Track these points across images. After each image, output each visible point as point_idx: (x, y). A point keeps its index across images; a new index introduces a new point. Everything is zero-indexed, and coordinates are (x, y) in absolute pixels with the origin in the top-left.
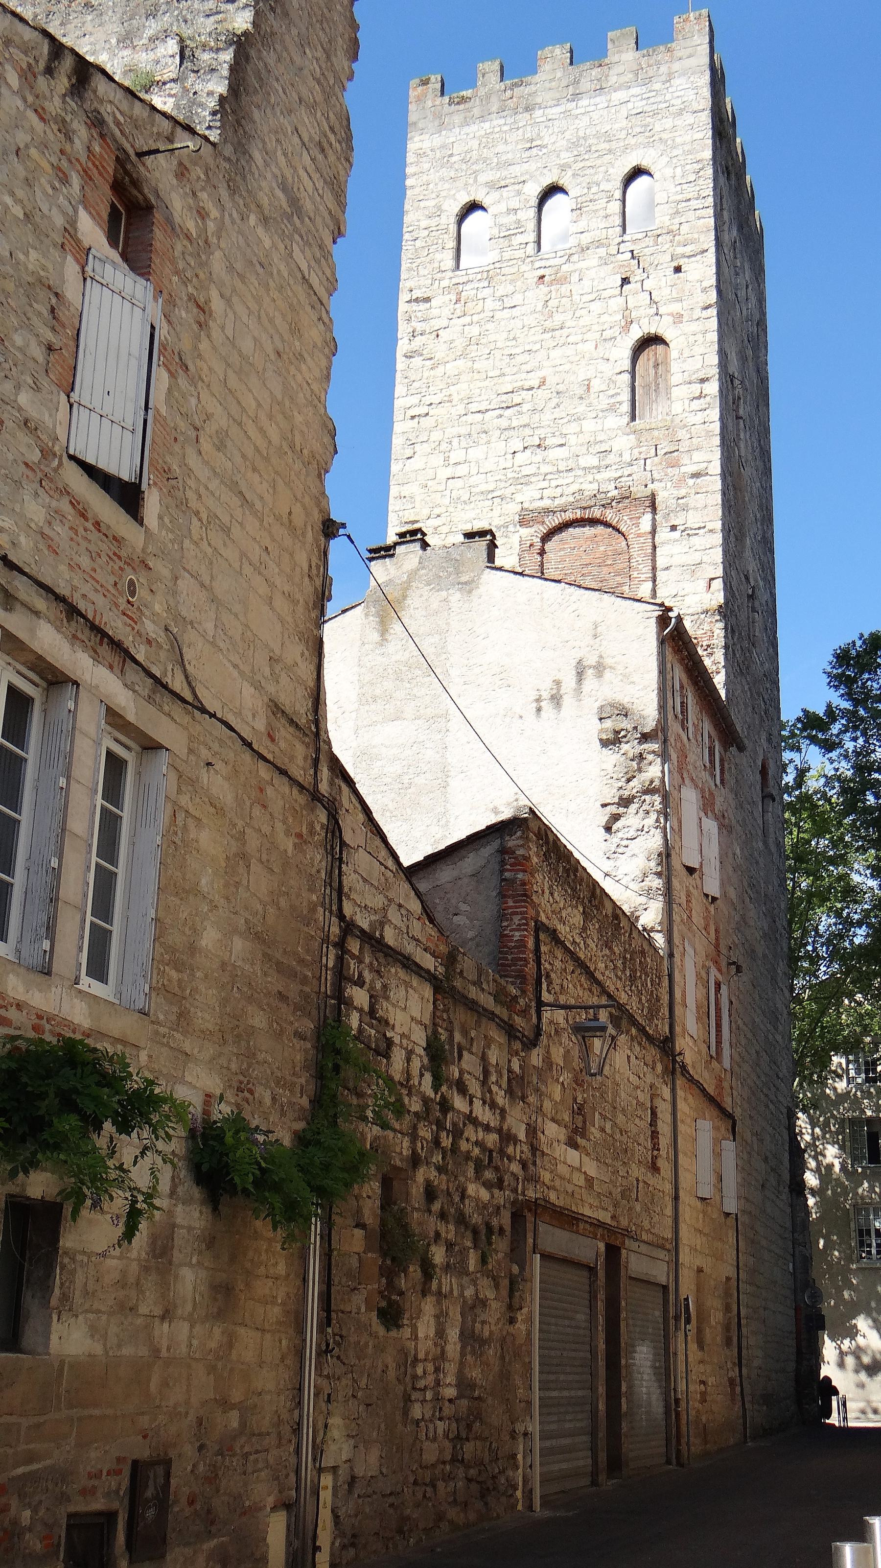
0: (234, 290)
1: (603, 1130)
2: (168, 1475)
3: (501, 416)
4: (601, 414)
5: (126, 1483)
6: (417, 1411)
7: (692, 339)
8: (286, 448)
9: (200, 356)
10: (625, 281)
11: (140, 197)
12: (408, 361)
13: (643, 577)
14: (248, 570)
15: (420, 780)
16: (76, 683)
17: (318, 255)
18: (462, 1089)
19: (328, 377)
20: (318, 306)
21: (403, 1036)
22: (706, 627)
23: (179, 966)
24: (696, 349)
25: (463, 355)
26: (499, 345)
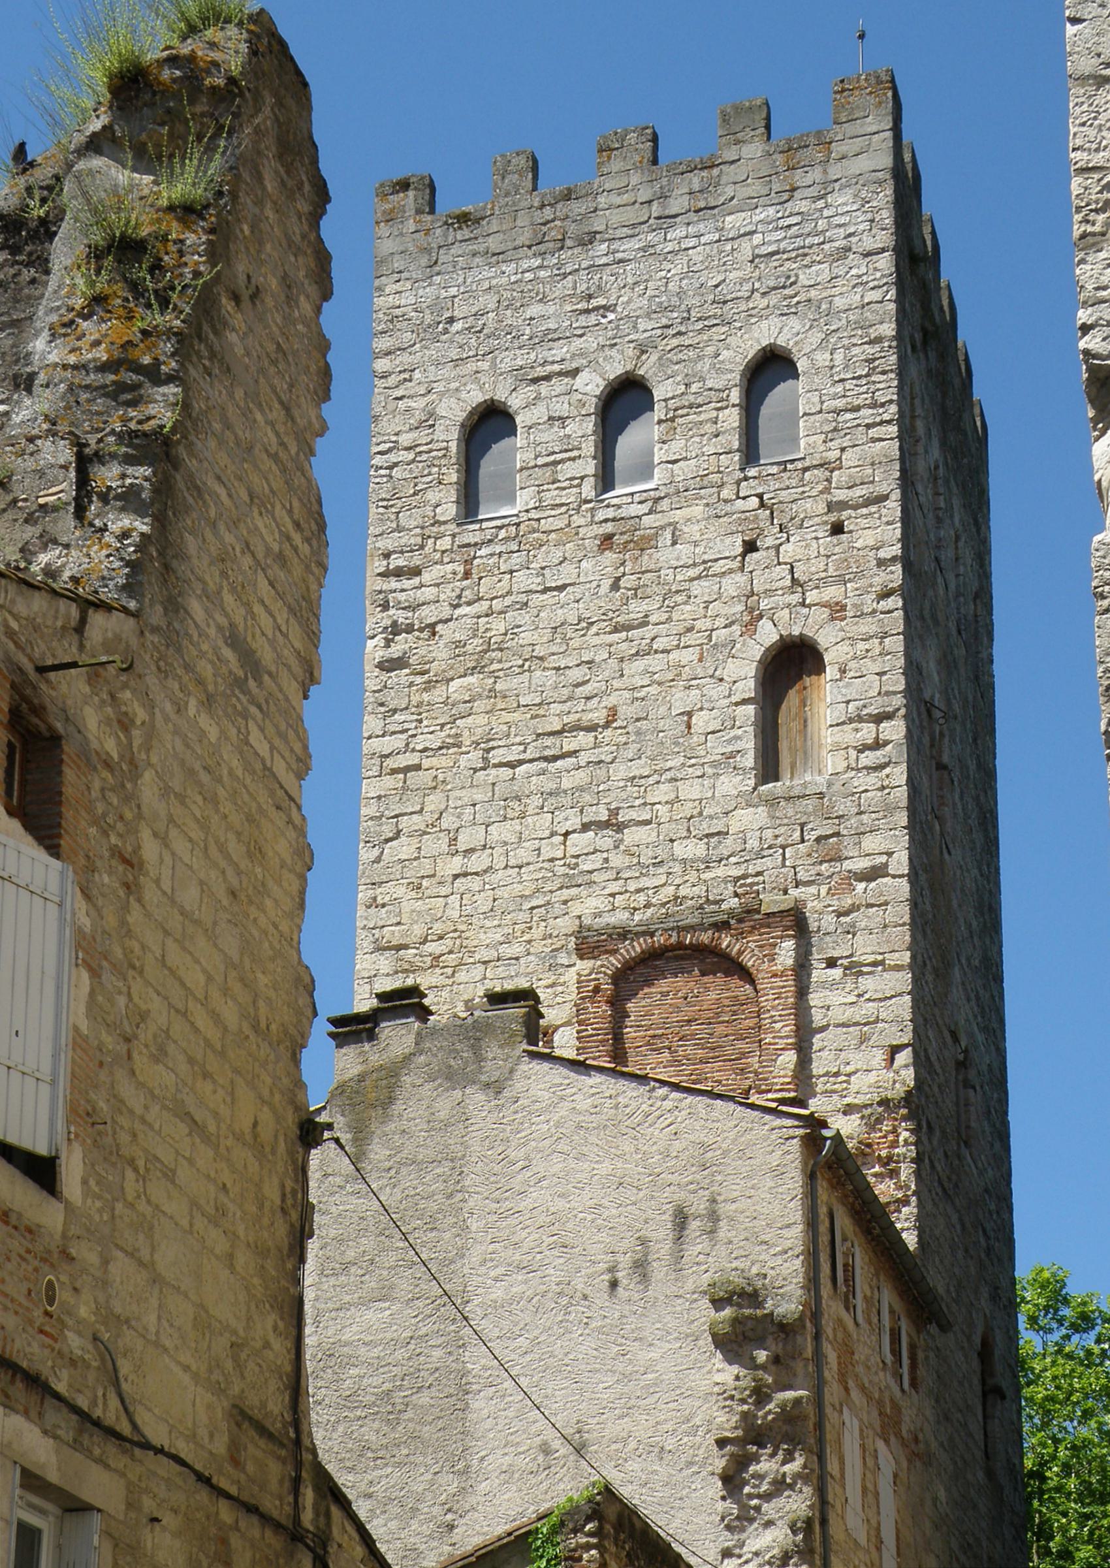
0: (171, 820)
3: (543, 772)
4: (710, 771)
8: (247, 1030)
9: (129, 933)
10: (750, 547)
11: (43, 727)
12: (384, 676)
13: (782, 1043)
14: (200, 1223)
15: (424, 1399)
17: (283, 726)
19: (302, 905)
20: (286, 803)
24: (864, 670)
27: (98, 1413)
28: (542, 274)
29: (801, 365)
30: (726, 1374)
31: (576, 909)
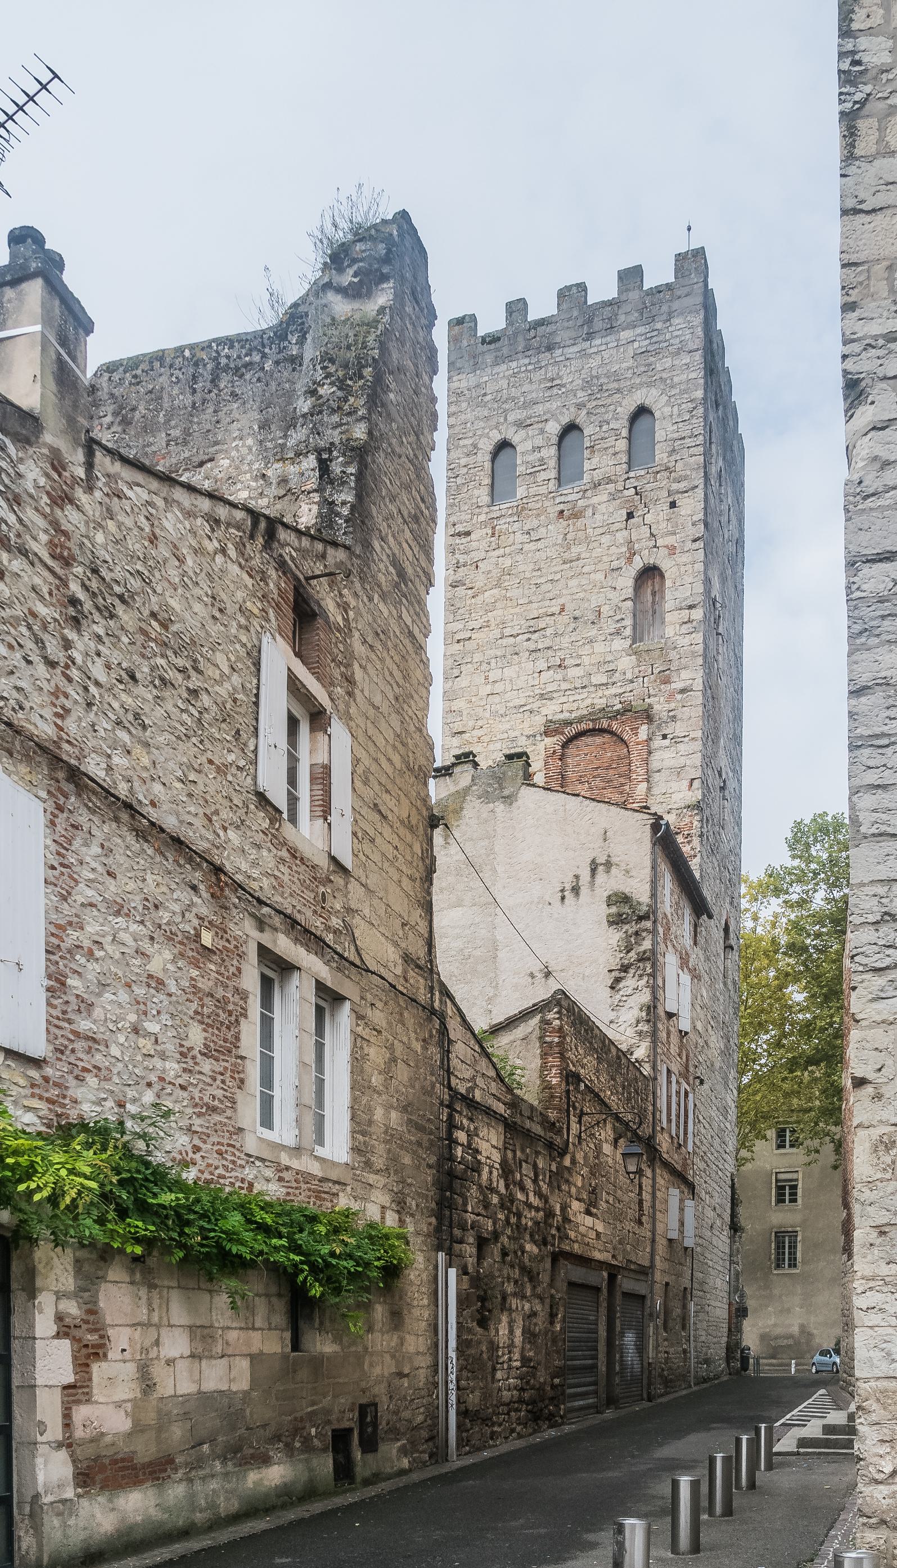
1: (607, 1202)
2: (376, 1412)
3: (529, 639)
5: (357, 1414)
6: (499, 1375)
7: (683, 569)
10: (630, 516)
14: (386, 865)
16: (299, 969)
18: (523, 1188)
21: (488, 1158)
22: (687, 820)
23: (364, 1133)
25: (496, 586)
26: (528, 575)
27: (346, 955)
28: (530, 367)
29: (657, 414)
30: (615, 936)
31: (544, 711)
